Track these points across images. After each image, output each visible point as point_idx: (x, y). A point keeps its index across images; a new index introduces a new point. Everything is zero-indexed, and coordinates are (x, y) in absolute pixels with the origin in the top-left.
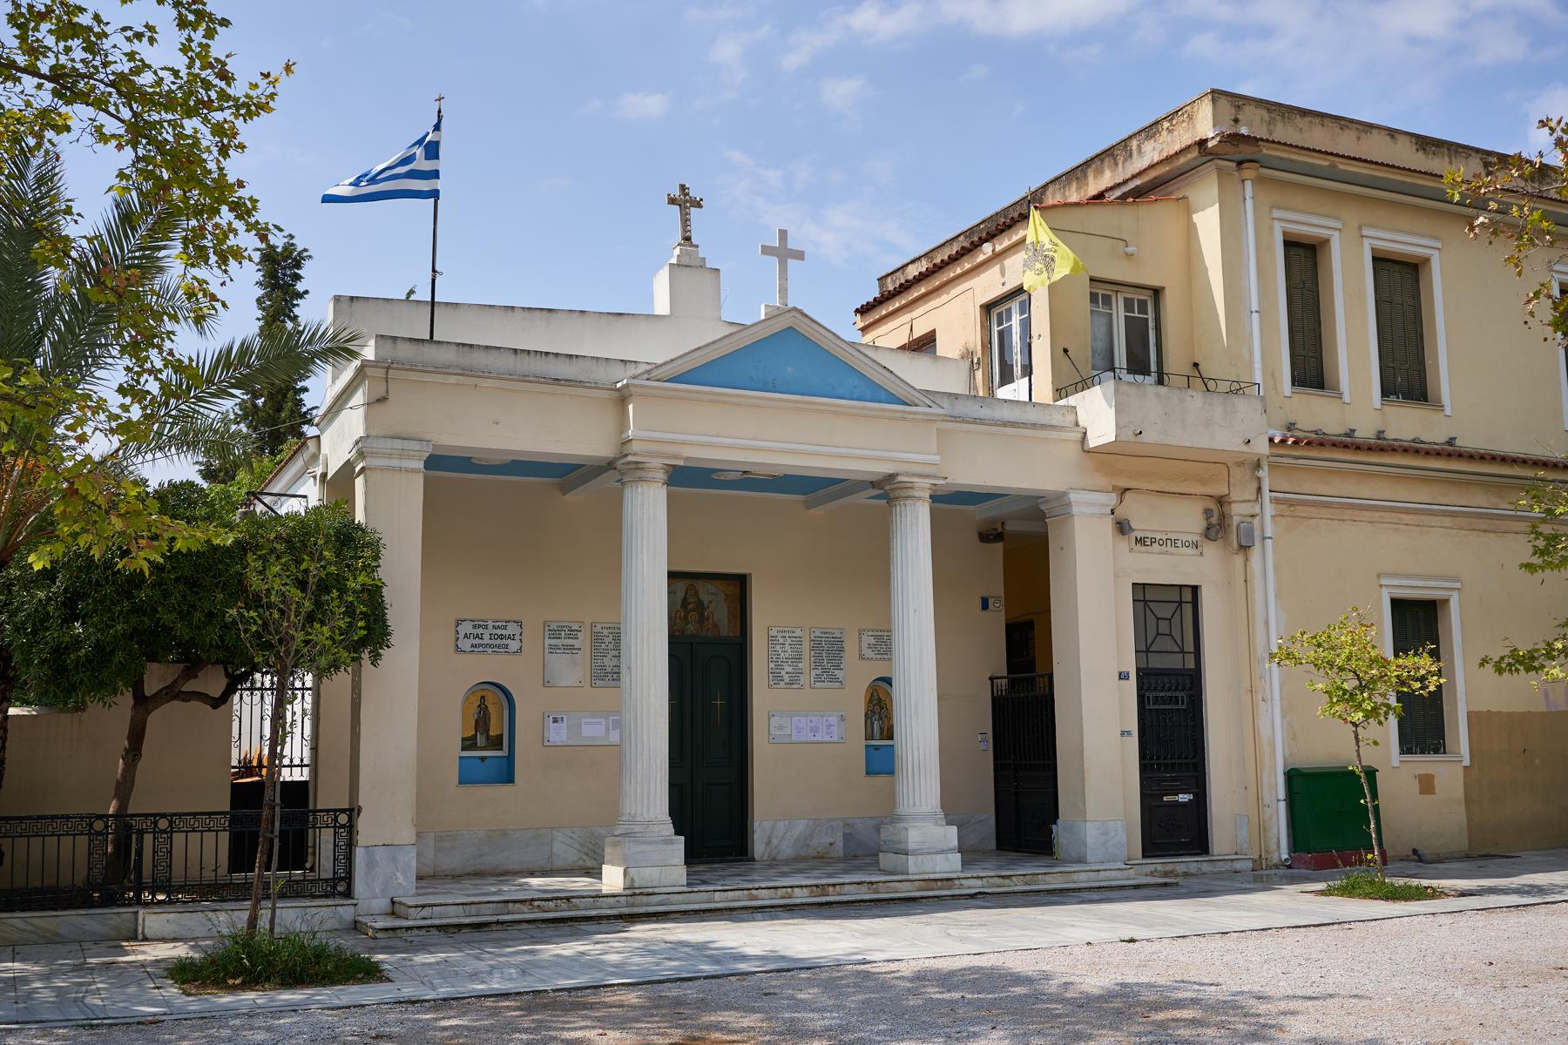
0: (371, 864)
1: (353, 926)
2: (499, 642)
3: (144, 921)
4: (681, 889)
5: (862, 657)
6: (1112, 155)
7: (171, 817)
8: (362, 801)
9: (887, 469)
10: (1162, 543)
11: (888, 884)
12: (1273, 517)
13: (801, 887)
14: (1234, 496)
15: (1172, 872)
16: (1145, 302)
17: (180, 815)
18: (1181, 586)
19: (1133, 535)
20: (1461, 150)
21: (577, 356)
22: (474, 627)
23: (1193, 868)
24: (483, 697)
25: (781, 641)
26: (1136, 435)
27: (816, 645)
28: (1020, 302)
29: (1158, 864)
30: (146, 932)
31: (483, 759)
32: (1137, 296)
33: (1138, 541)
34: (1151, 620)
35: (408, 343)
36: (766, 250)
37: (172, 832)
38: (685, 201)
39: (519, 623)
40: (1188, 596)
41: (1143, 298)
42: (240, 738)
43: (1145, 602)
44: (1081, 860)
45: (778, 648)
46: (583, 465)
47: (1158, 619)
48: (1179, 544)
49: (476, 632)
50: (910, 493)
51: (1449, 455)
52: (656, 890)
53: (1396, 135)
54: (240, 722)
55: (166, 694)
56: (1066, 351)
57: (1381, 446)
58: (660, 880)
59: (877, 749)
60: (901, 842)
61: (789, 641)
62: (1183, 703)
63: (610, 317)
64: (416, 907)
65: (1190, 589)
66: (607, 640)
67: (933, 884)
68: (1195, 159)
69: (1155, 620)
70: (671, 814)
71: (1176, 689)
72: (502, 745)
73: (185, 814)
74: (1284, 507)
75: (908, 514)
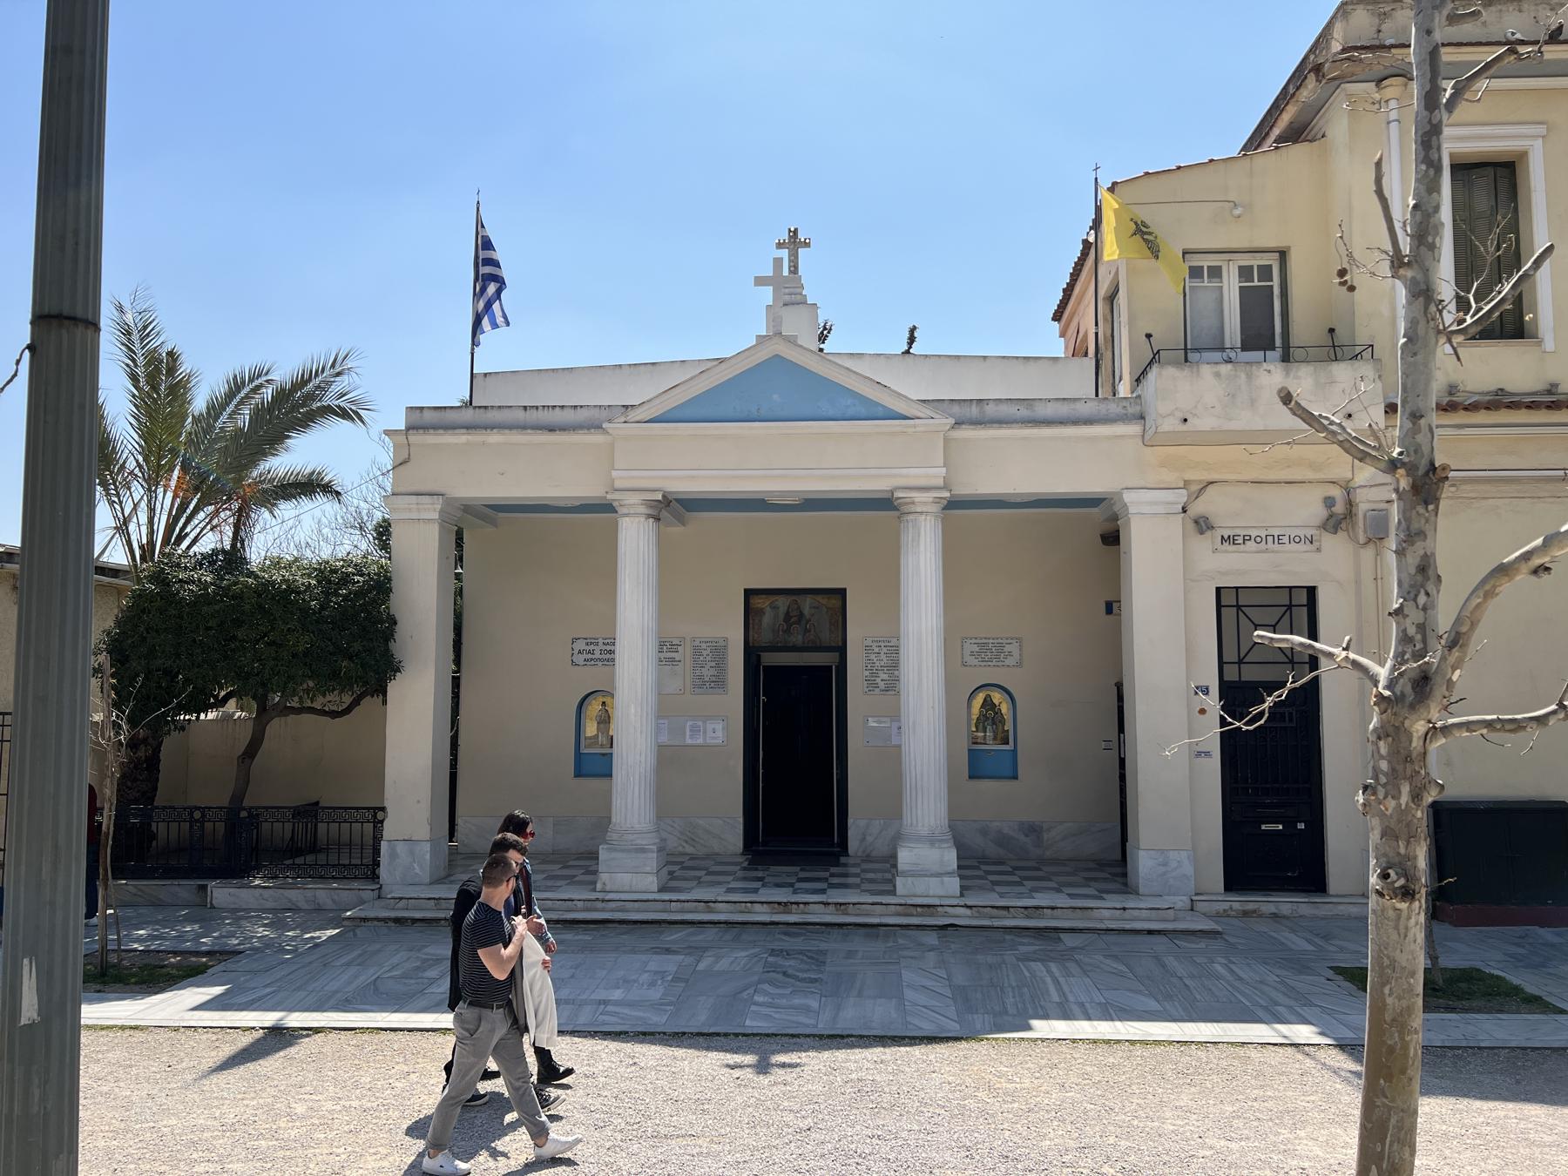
0: (393, 855)
3: (212, 892)
4: (651, 897)
15: (1255, 911)
16: (1270, 267)
19: (1218, 533)
21: (581, 407)
22: (587, 644)
23: (1285, 909)
24: (604, 703)
29: (1237, 902)
30: (213, 902)
32: (1256, 261)
45: (873, 657)
48: (1286, 539)
49: (588, 648)
50: (913, 509)
58: (631, 886)
61: (885, 650)
62: (1291, 720)
67: (913, 910)
73: (259, 808)
75: (910, 529)
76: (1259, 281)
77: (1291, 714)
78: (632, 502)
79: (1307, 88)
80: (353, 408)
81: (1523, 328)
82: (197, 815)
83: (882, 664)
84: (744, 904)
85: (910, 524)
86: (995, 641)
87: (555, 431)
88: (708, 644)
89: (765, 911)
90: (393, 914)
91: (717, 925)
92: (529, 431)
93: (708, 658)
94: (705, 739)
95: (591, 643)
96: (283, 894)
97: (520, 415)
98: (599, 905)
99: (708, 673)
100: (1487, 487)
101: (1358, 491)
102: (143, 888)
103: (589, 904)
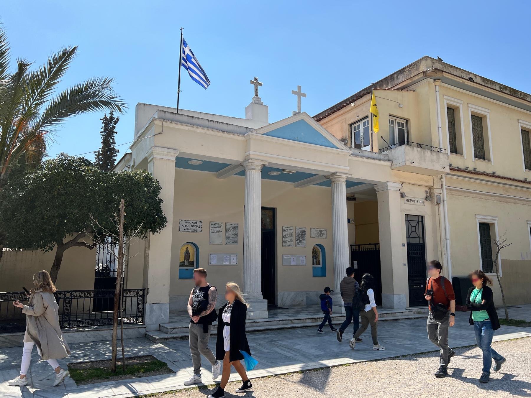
0: (152, 311)
1: (144, 336)
2: (194, 228)
5: (311, 237)
6: (387, 80)
7: (71, 292)
8: (150, 286)
9: (333, 170)
10: (414, 201)
11: (337, 318)
12: (446, 194)
13: (309, 319)
14: (435, 187)
15: (420, 312)
17: (75, 291)
18: (418, 216)
19: (405, 198)
20: (494, 83)
21: (230, 124)
24: (187, 248)
25: (287, 231)
26: (412, 163)
27: (297, 233)
28: (364, 123)
29: (415, 309)
31: (187, 269)
32: (402, 121)
33: (407, 200)
34: (410, 226)
35: (170, 114)
36: (294, 92)
37: (72, 298)
38: (256, 83)
39: (201, 222)
40: (420, 219)
41: (403, 122)
42: (99, 261)
43: (408, 220)
44: (392, 308)
45: (285, 233)
46: (229, 165)
47: (412, 226)
49: (186, 224)
51: (493, 176)
52: (258, 321)
53: (477, 76)
54: (99, 255)
55: (72, 243)
56: (382, 137)
57: (475, 172)
59: (315, 268)
60: (337, 302)
63: (233, 119)
64: (171, 329)
65: (421, 217)
66: (230, 228)
68: (421, 77)
69: (411, 227)
70: (262, 291)
71: (418, 250)
72: (193, 264)
73: (78, 291)
74: (449, 191)
76: (402, 127)
77: (419, 253)
78: (257, 164)
79: (418, 77)
80: (117, 105)
81: (456, 151)
82: (68, 295)
83: (288, 236)
84: (303, 320)
85: (339, 185)
86: (320, 230)
87: (225, 132)
88: (232, 225)
89: (310, 322)
90: (180, 335)
91: (303, 328)
92: (215, 130)
93: (232, 231)
94: (230, 263)
95: (188, 222)
96: (98, 334)
97: (207, 123)
98: (255, 324)
99: (231, 236)
100: (456, 192)
101: (435, 190)
102: (8, 337)
103: (251, 324)
